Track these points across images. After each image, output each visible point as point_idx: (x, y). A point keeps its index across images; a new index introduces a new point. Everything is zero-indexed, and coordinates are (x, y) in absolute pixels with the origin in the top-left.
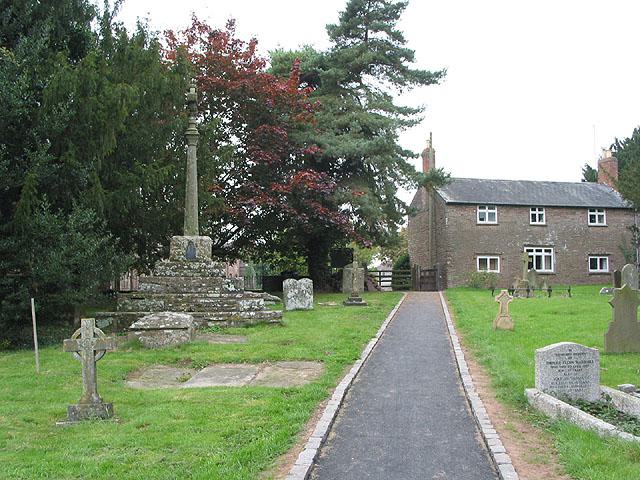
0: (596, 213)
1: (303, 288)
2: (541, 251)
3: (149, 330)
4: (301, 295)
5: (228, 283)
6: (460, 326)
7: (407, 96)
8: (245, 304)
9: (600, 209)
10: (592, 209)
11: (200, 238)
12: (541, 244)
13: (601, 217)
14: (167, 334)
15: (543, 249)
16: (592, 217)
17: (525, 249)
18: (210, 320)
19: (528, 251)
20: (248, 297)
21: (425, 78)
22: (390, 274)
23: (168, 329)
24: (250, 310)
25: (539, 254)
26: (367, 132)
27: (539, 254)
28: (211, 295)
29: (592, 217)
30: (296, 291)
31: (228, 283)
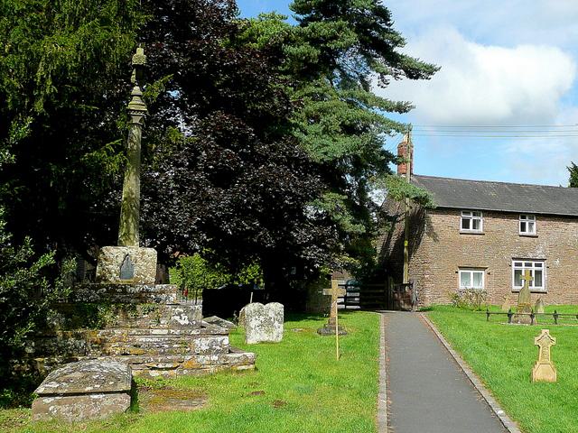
0: (472, 218)
1: (271, 314)
2: (520, 265)
3: (65, 395)
4: (267, 324)
5: (179, 314)
6: (387, 344)
7: (397, 88)
8: (202, 344)
9: (476, 213)
10: (467, 211)
11: (140, 250)
12: (531, 256)
13: (476, 224)
14: (95, 401)
15: (533, 263)
16: (523, 226)
17: (514, 262)
18: (154, 368)
19: (517, 264)
20: (208, 334)
21: (414, 72)
22: (358, 294)
23: (98, 393)
24: (208, 352)
25: (518, 268)
26: (349, 129)
27: (518, 268)
28: (155, 332)
29: (523, 226)
30: (262, 318)
31: (179, 314)
